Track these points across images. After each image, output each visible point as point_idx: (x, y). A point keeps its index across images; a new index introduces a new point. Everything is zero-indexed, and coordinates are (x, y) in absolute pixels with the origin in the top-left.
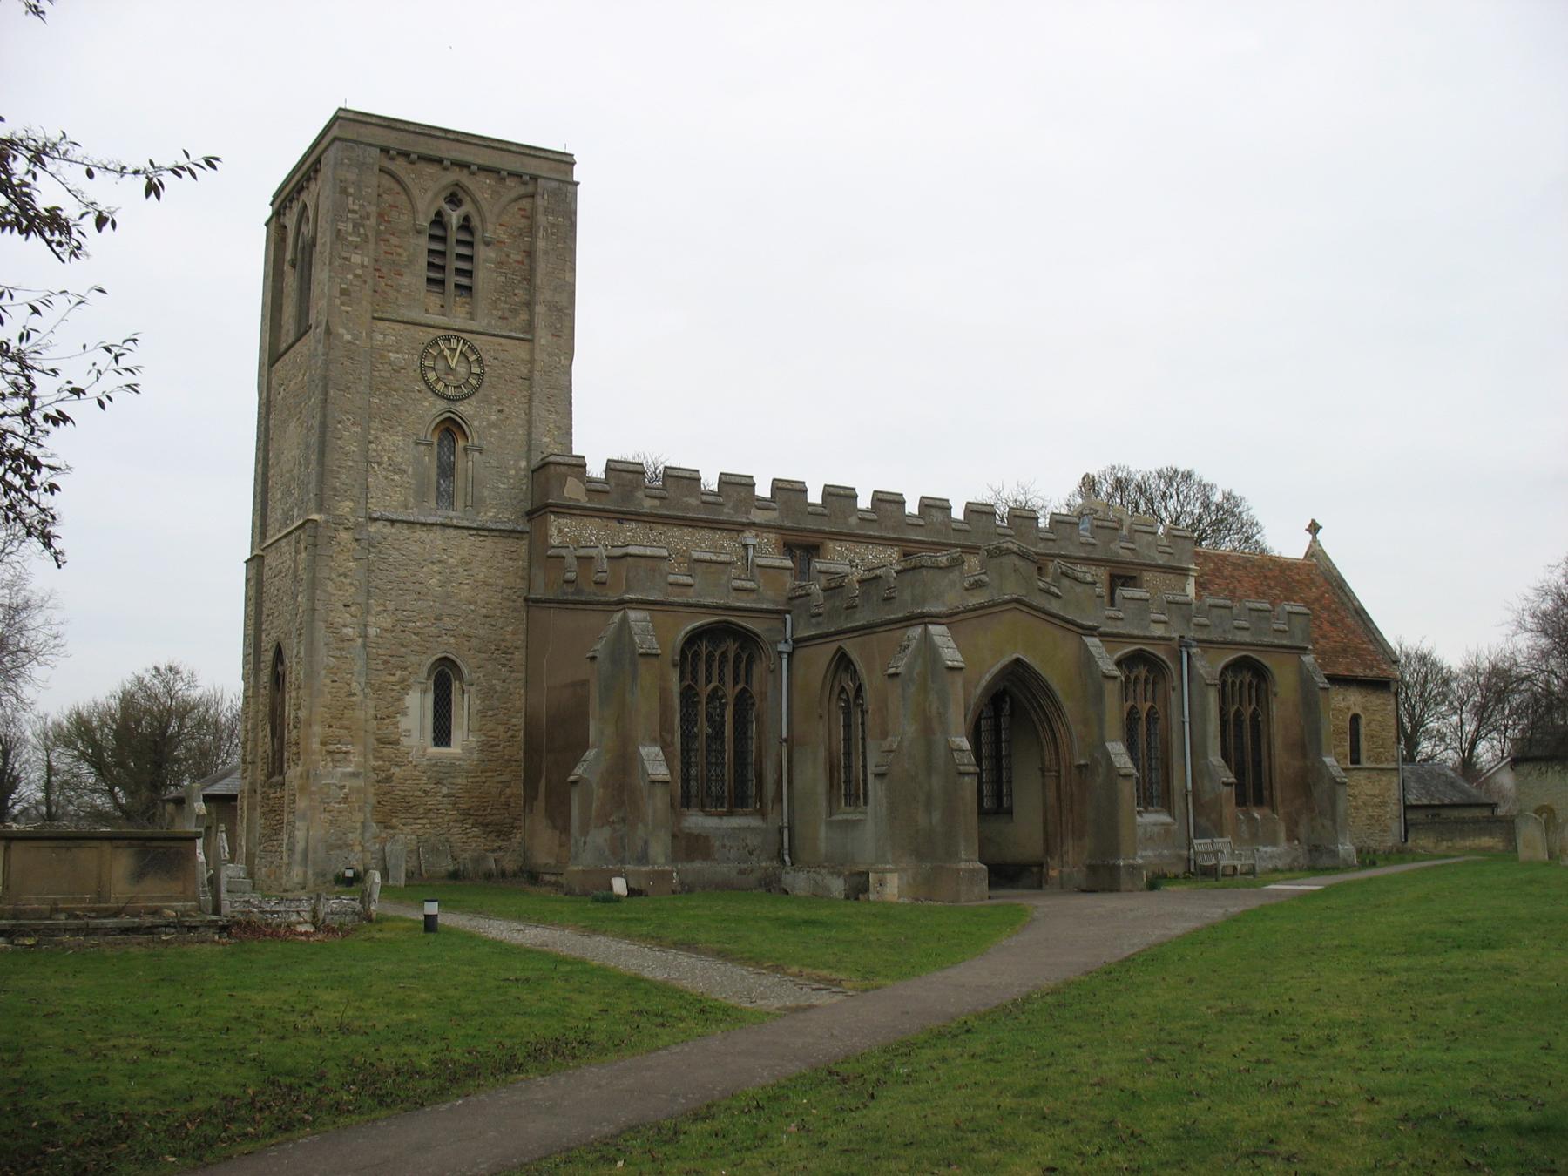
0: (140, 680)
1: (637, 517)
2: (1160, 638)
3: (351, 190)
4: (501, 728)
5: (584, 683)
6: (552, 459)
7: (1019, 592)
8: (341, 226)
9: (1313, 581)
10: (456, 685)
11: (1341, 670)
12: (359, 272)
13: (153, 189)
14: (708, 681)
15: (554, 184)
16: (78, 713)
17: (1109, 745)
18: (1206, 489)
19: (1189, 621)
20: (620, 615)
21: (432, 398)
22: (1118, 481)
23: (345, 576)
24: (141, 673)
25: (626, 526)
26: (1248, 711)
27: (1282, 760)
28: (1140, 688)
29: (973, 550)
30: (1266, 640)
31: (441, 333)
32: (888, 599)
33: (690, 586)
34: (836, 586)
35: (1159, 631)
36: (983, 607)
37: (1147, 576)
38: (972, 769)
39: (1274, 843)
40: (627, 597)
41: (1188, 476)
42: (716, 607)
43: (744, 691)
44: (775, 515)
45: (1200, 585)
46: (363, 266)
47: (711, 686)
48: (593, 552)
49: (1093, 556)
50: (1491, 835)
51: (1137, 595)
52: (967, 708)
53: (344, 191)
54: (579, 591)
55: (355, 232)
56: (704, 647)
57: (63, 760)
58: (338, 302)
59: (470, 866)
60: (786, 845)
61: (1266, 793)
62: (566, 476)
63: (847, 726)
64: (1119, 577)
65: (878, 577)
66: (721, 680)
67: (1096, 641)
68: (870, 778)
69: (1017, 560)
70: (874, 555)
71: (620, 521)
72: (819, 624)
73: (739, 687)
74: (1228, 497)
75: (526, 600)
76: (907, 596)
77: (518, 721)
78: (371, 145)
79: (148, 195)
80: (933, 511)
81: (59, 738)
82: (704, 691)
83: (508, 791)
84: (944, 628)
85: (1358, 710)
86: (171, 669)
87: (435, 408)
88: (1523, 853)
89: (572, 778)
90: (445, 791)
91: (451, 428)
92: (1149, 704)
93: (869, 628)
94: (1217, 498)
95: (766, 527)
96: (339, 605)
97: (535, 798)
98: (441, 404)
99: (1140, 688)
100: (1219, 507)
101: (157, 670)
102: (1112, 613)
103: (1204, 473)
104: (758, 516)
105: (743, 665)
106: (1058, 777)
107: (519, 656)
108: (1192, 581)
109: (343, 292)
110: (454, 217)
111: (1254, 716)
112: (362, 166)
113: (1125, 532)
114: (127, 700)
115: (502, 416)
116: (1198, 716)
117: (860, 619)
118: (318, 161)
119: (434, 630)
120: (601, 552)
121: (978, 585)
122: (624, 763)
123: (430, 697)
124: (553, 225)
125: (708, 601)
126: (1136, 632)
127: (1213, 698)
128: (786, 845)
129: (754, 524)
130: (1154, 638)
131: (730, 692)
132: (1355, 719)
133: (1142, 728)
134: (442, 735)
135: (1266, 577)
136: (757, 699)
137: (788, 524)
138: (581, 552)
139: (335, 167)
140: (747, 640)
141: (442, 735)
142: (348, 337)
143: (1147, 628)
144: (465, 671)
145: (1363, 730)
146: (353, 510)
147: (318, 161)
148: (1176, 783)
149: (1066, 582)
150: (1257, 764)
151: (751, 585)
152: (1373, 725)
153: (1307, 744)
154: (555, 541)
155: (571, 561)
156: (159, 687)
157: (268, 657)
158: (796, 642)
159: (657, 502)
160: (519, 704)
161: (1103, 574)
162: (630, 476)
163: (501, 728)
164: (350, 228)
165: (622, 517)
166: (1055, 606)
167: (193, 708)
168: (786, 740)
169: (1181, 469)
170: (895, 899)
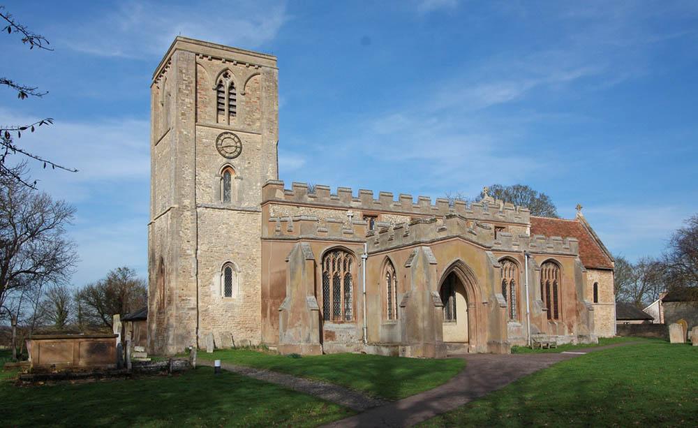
0: (113, 273)
1: (306, 205)
2: (516, 252)
3: (184, 71)
4: (252, 289)
5: (284, 271)
6: (270, 182)
7: (459, 233)
8: (180, 86)
9: (578, 229)
10: (233, 273)
11: (589, 265)
12: (189, 106)
13: (23, 95)
14: (334, 270)
15: (268, 69)
16: (92, 288)
17: (496, 295)
18: (532, 193)
19: (528, 245)
20: (298, 243)
21: (221, 157)
22: (497, 191)
23: (187, 229)
24: (113, 270)
25: (301, 208)
26: (551, 282)
27: (566, 303)
28: (507, 272)
29: (441, 217)
30: (560, 252)
31: (224, 131)
32: (406, 236)
33: (326, 232)
34: (384, 231)
35: (515, 248)
36: (444, 239)
37: (510, 227)
38: (440, 305)
39: (563, 333)
40: (300, 237)
41: (525, 188)
42: (337, 240)
43: (348, 273)
44: (360, 203)
45: (532, 231)
46: (190, 103)
47: (335, 272)
48: (287, 219)
49: (488, 219)
50: (653, 331)
51: (507, 234)
52: (438, 278)
53: (181, 71)
54: (282, 235)
55: (186, 89)
56: (331, 256)
57: (83, 303)
58: (180, 118)
59: (240, 344)
60: (365, 335)
61: (559, 314)
62: (276, 189)
63: (390, 287)
64: (498, 227)
65: (402, 227)
66: (339, 269)
67: (491, 252)
68: (399, 308)
69: (457, 219)
70: (399, 219)
71: (298, 207)
72: (378, 247)
73: (346, 272)
74: (542, 196)
75: (262, 239)
76: (414, 235)
77: (259, 287)
78: (192, 52)
79: (19, 97)
80: (423, 202)
81: (80, 296)
82: (331, 274)
83: (255, 314)
84: (428, 248)
85: (597, 281)
86: (125, 268)
87: (222, 161)
88: (673, 340)
89: (280, 309)
90: (230, 315)
91: (227, 171)
92: (511, 278)
93: (398, 248)
94: (537, 196)
95: (357, 208)
96: (186, 241)
97: (266, 317)
98: (225, 160)
99: (507, 272)
100: (538, 200)
101: (120, 269)
102: (496, 241)
103: (533, 187)
104: (354, 204)
105: (336, 264)
106: (475, 307)
107: (259, 261)
108: (528, 229)
109: (183, 114)
110: (227, 83)
111: (555, 283)
112: (188, 60)
113: (501, 210)
114: (110, 281)
115: (249, 165)
116: (532, 282)
117: (395, 244)
118: (170, 59)
119: (224, 251)
120: (290, 219)
121: (443, 230)
122: (302, 302)
123: (223, 277)
124: (268, 86)
125: (333, 237)
126: (506, 249)
127: (538, 274)
128: (365, 335)
129: (351, 208)
130: (513, 252)
131: (342, 275)
132: (596, 285)
133: (508, 288)
134: (228, 292)
135: (559, 228)
136: (353, 277)
137: (365, 207)
138: (282, 219)
139: (177, 61)
140: (348, 252)
141: (228, 292)
142: (185, 133)
143: (511, 247)
144: (237, 267)
145: (599, 289)
146: (190, 203)
147: (170, 59)
148: (522, 310)
149: (479, 228)
150: (556, 302)
151: (351, 231)
152: (603, 287)
153: (579, 294)
154: (272, 215)
155: (278, 222)
156: (120, 277)
157: (158, 263)
158: (369, 254)
159: (313, 199)
160: (259, 280)
161: (492, 226)
162: (302, 189)
163: (252, 289)
164: (184, 87)
165: (299, 205)
166: (474, 238)
167: (134, 284)
168: (365, 293)
169: (522, 185)
170: (410, 357)
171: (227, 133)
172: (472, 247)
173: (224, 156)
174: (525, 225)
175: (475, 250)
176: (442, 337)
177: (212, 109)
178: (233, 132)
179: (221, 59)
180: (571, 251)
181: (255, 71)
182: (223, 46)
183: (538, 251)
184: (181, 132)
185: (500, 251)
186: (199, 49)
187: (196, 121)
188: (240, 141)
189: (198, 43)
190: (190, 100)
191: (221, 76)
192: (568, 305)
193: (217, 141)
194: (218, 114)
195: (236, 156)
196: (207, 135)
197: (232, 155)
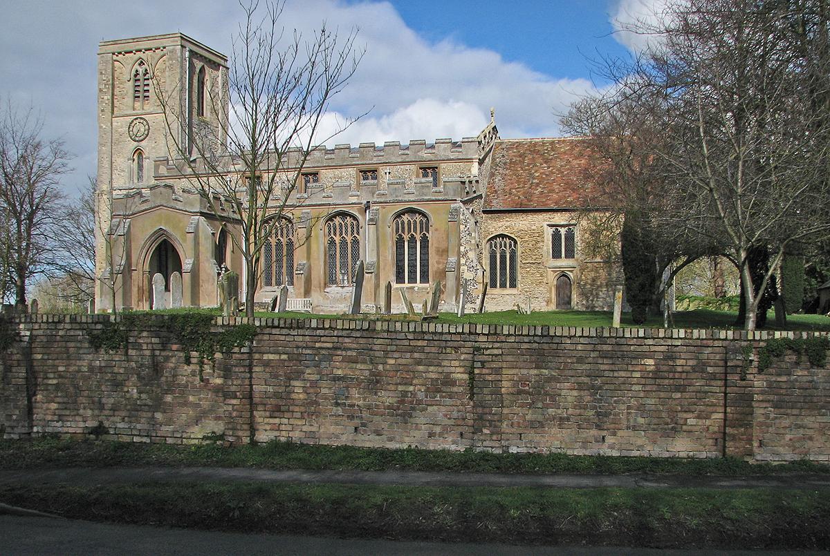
31: (135, 117)
35: (354, 200)
56: (406, 218)
62: (159, 165)
109: (102, 111)
115: (156, 144)
131: (349, 239)
142: (104, 127)
171: (136, 119)
172: (178, 214)
173: (135, 141)
174: (470, 160)
175: (181, 216)
176: (612, 324)
177: (129, 100)
178: (142, 116)
179: (151, 50)
180: (446, 194)
181: (162, 53)
182: (134, 39)
183: (388, 200)
184: (101, 127)
185: (329, 205)
186: (116, 48)
187: (113, 113)
188: (148, 124)
189: (115, 43)
190: (108, 97)
191: (137, 67)
192: (436, 265)
193: (129, 128)
194: (134, 101)
195: (145, 138)
196: (120, 124)
197: (141, 139)
